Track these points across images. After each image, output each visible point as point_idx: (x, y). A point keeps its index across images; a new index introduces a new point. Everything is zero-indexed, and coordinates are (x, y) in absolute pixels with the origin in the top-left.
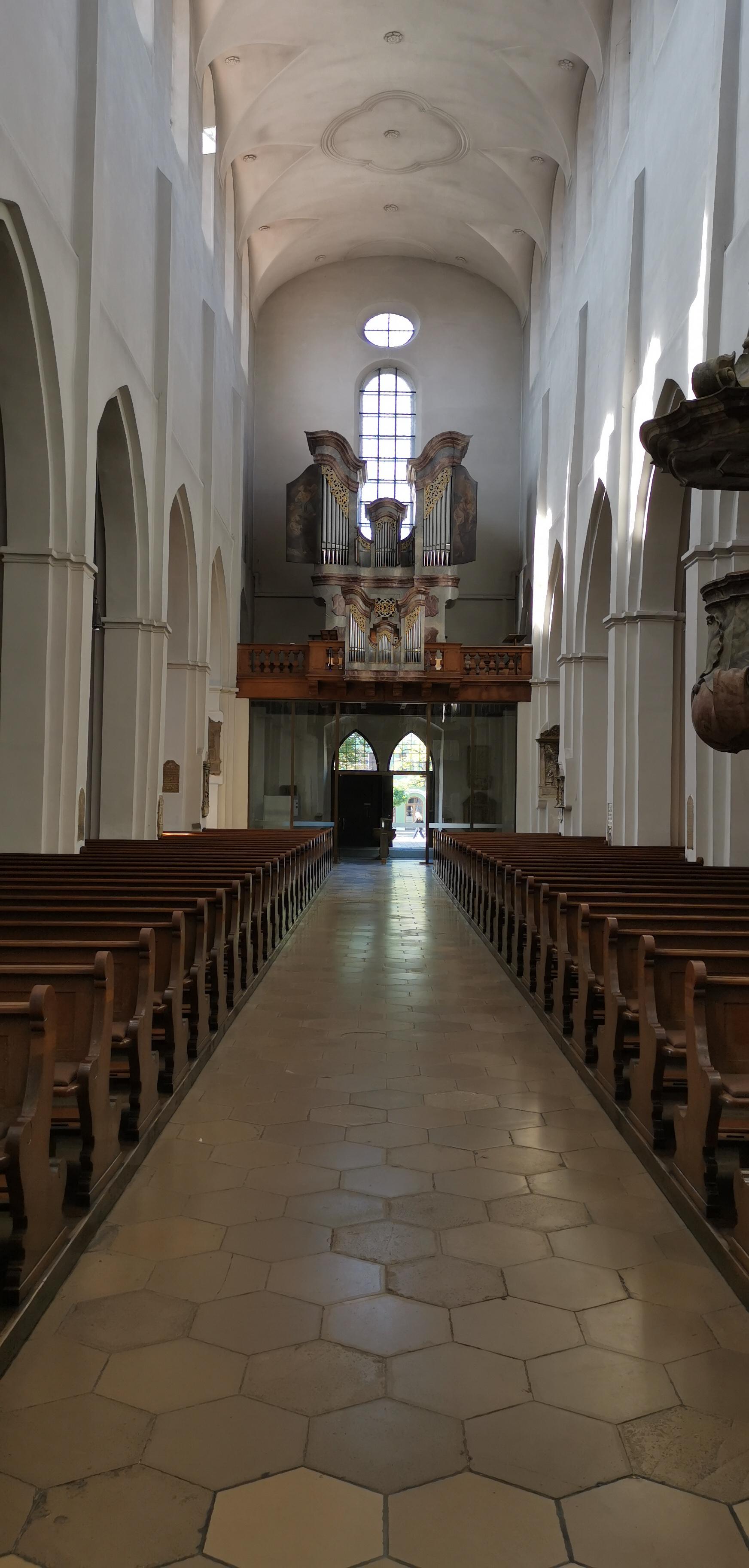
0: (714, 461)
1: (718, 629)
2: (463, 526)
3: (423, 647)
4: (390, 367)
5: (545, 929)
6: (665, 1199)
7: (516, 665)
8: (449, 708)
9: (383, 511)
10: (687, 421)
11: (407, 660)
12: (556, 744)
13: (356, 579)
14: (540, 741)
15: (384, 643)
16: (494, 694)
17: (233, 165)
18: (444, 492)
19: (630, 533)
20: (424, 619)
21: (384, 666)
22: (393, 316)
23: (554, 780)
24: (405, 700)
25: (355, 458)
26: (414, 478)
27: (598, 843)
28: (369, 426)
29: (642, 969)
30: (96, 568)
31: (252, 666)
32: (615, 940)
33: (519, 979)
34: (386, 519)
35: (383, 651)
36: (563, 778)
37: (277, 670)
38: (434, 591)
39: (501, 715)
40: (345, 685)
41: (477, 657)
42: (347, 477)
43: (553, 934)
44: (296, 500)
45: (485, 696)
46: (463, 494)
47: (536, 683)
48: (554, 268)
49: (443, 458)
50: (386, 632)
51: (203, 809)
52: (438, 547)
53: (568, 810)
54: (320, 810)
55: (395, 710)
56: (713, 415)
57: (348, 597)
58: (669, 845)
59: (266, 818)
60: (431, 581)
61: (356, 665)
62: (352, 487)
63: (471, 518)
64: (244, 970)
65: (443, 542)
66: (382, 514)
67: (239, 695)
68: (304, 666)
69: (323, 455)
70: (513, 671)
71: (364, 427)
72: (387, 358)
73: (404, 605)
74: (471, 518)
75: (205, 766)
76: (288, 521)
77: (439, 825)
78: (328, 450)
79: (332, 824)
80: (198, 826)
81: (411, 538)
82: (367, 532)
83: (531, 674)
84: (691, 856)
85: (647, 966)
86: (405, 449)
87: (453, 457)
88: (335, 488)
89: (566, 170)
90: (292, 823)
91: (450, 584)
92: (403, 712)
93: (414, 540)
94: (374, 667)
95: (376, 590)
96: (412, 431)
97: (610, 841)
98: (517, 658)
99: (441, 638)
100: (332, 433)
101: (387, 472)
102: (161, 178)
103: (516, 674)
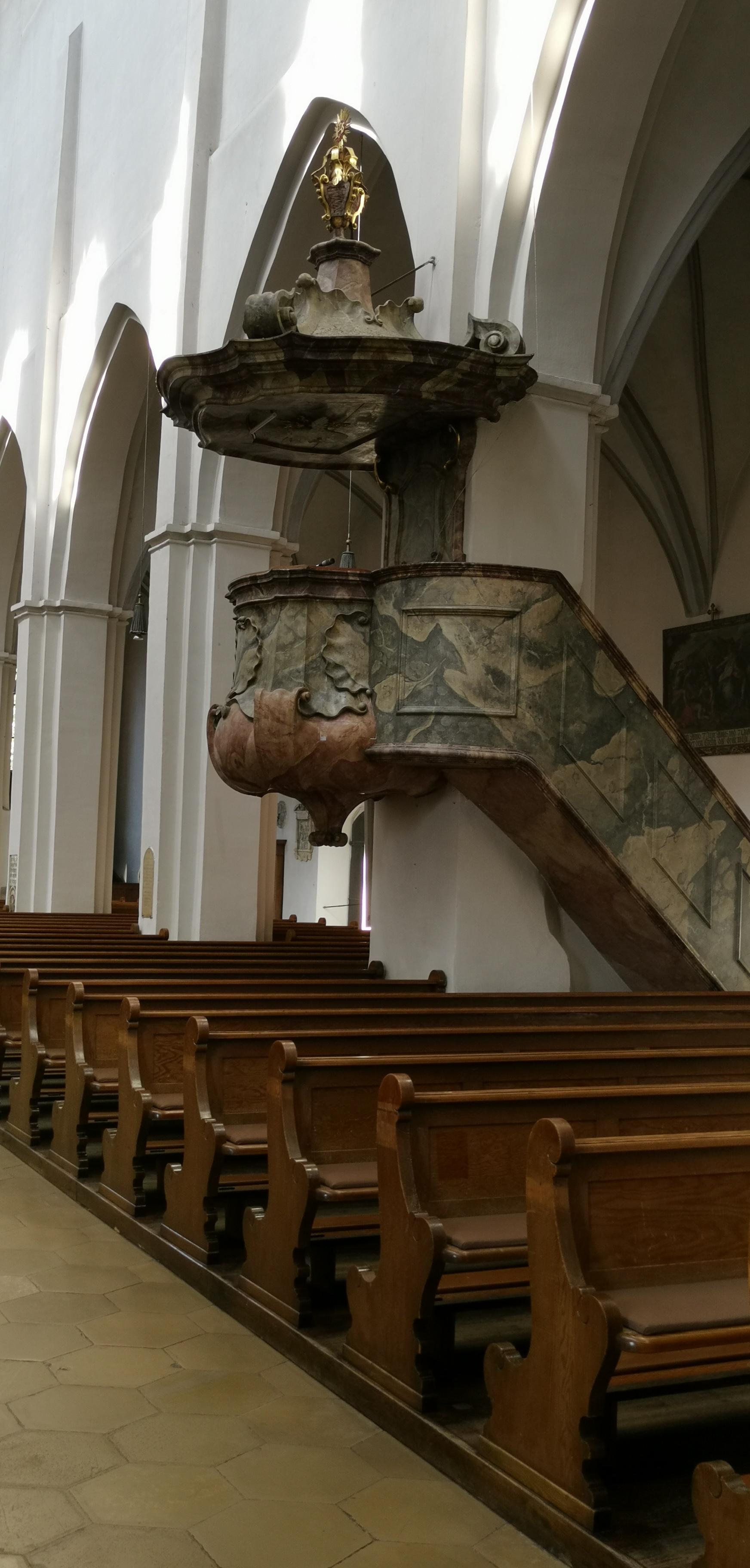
0: (250, 422)
1: (255, 636)
6: (333, 1396)
10: (235, 365)
19: (54, 498)
58: (91, 911)
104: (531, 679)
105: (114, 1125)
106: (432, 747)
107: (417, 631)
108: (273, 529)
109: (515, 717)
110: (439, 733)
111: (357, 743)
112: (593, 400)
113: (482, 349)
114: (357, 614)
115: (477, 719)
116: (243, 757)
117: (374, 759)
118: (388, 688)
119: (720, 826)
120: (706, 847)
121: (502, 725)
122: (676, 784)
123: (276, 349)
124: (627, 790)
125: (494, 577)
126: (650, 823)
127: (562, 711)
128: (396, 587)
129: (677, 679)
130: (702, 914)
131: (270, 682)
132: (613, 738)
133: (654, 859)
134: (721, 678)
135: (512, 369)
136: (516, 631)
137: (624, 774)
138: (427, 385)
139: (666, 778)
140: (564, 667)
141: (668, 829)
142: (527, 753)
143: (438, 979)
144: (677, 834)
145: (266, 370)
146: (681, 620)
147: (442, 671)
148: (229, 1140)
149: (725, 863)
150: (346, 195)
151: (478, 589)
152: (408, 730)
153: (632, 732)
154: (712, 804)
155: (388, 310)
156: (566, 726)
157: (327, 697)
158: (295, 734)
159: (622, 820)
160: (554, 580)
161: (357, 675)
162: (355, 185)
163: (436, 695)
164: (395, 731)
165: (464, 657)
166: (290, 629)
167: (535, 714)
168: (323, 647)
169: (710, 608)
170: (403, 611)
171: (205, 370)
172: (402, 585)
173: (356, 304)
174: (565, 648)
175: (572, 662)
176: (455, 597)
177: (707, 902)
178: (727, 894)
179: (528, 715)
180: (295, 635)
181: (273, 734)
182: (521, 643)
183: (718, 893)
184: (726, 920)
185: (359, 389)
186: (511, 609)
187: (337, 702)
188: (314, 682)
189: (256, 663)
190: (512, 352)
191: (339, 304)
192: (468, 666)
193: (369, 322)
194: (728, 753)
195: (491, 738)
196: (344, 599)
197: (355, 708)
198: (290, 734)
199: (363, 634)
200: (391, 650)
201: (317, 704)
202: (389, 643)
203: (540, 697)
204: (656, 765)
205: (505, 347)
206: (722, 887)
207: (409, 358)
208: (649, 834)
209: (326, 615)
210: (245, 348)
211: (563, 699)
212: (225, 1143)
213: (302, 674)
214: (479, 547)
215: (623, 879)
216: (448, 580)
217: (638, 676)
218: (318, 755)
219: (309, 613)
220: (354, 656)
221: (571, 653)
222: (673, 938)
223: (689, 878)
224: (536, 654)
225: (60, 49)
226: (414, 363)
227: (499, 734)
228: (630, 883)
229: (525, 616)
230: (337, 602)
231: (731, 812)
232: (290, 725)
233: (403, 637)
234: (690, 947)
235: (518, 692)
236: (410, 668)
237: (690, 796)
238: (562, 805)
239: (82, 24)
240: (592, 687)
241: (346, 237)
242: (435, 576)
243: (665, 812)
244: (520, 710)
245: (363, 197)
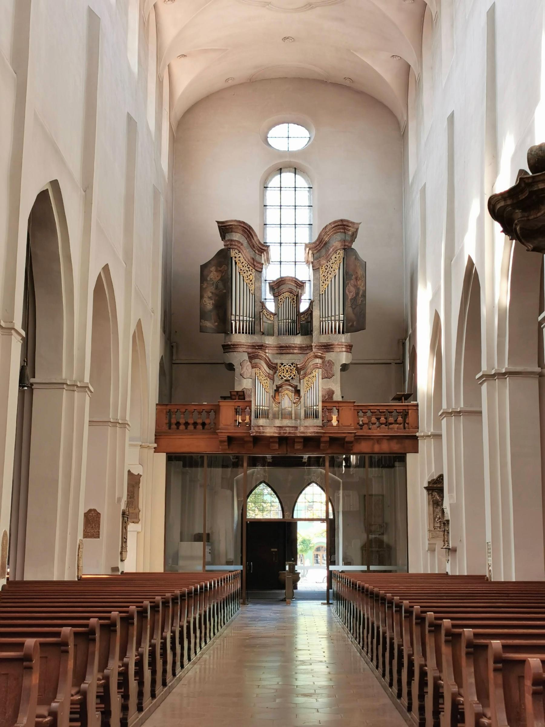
2: (354, 299)
3: (320, 404)
4: (290, 167)
5: (417, 648)
7: (405, 422)
8: (347, 460)
9: (284, 288)
10: (526, 194)
11: (306, 416)
12: (441, 491)
13: (262, 347)
14: (427, 489)
15: (287, 401)
16: (385, 447)
17: (155, 6)
18: (337, 271)
20: (320, 380)
21: (286, 422)
22: (291, 125)
23: (441, 524)
24: (305, 452)
25: (260, 243)
26: (311, 259)
27: (482, 579)
28: (272, 216)
29: (491, 674)
30: (23, 333)
31: (170, 424)
32: (500, 665)
33: (398, 701)
34: (287, 294)
35: (285, 409)
36: (448, 521)
37: (191, 427)
38: (329, 356)
39: (393, 466)
40: (251, 439)
41: (369, 414)
42: (253, 259)
43: (424, 654)
44: (209, 279)
45: (377, 448)
46: (353, 272)
47: (423, 437)
48: (426, 85)
49: (336, 242)
50: (287, 392)
51: (121, 553)
52: (333, 318)
53: (452, 551)
54: (231, 556)
55: (298, 463)
57: (253, 361)
59: (181, 563)
60: (327, 347)
61: (262, 422)
62: (257, 267)
63: (361, 293)
64: (140, 694)
65: (337, 313)
66: (284, 290)
67: (156, 450)
68: (215, 423)
69: (232, 240)
70: (402, 426)
71: (267, 218)
72: (287, 160)
73: (302, 368)
74: (361, 293)
75: (124, 513)
76: (202, 297)
77: (339, 567)
78: (237, 236)
79: (240, 568)
80: (116, 569)
81: (309, 312)
82: (271, 306)
83: (418, 428)
85: (495, 670)
86: (305, 236)
87: (345, 241)
88: (242, 269)
90: (204, 567)
91: (344, 349)
92: (303, 464)
93: (312, 312)
94: (278, 423)
95: (279, 356)
96: (310, 220)
97: (490, 577)
98: (405, 415)
99: (337, 397)
100: (239, 222)
101: (288, 256)
102: (91, 14)
103: (405, 428)
105: (443, 712)
148: (486, 716)
210: (530, 181)
212: (482, 718)
225: (482, 21)
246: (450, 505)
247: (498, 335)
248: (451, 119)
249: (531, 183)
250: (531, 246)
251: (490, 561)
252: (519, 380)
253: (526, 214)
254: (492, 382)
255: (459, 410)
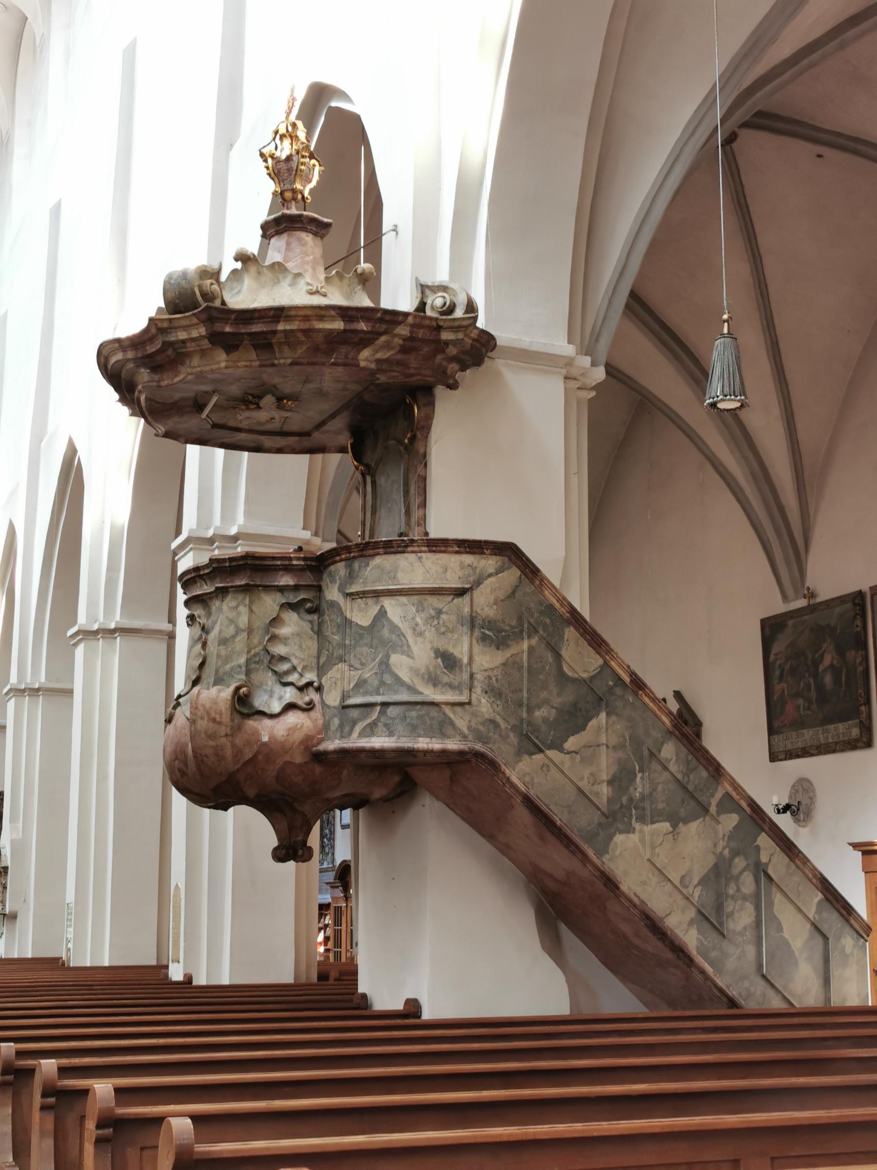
27: (55, 963)
29: (36, 1115)
32: (52, 1100)
36: (6, 869)
48: (19, 150)
56: (193, 340)
84: (176, 973)
89: (35, 25)
104: (487, 660)
106: (379, 742)
107: (361, 615)
108: (304, 529)
109: (469, 703)
110: (386, 725)
111: (302, 742)
112: (569, 362)
113: (429, 312)
114: (304, 601)
115: (426, 708)
116: (186, 765)
117: (320, 757)
118: (334, 680)
119: (731, 821)
120: (715, 845)
121: (454, 713)
122: (672, 773)
123: (197, 324)
124: (610, 783)
125: (441, 552)
126: (642, 819)
127: (525, 695)
128: (340, 569)
129: (777, 672)
130: (712, 919)
131: (212, 680)
132: (590, 724)
133: (649, 860)
134: (821, 668)
135: (457, 332)
136: (467, 610)
137: (605, 765)
138: (365, 353)
139: (659, 768)
140: (525, 646)
141: (666, 826)
142: (484, 743)
143: (413, 1008)
144: (677, 830)
145: (191, 347)
146: (779, 607)
147: (388, 657)
149: (740, 863)
150: (295, 168)
151: (424, 566)
152: (354, 723)
153: (614, 718)
154: (719, 795)
155: (336, 280)
156: (530, 711)
157: (271, 694)
158: (232, 735)
159: (607, 817)
160: (508, 552)
161: (305, 668)
162: (303, 157)
163: (382, 683)
164: (341, 726)
165: (411, 640)
166: (231, 621)
167: (492, 699)
168: (267, 638)
169: (806, 592)
170: (347, 594)
171: (134, 352)
172: (346, 567)
173: (298, 275)
174: (526, 625)
175: (534, 641)
176: (400, 575)
177: (719, 908)
178: (745, 898)
179: (483, 701)
180: (237, 627)
181: (212, 736)
182: (472, 622)
183: (733, 897)
184: (745, 928)
185: (289, 361)
186: (460, 586)
187: (281, 698)
188: (256, 678)
189: (200, 661)
190: (459, 313)
191: (281, 276)
192: (415, 649)
193: (311, 293)
194: (834, 751)
195: (443, 728)
196: (288, 586)
197: (300, 703)
198: (226, 735)
199: (311, 622)
200: (336, 637)
201: (260, 702)
202: (334, 630)
203: (497, 680)
204: (646, 753)
205: (451, 309)
206: (738, 890)
207: (339, 325)
208: (641, 831)
209: (270, 603)
210: (165, 325)
211: (525, 682)
213: (244, 669)
214: (442, 521)
215: (610, 883)
216: (391, 558)
217: (616, 654)
218: (260, 757)
219: (251, 603)
220: (300, 647)
221: (533, 631)
222: (679, 950)
223: (695, 881)
224: (491, 634)
226: (345, 331)
227: (451, 723)
228: (618, 888)
229: (477, 593)
230: (281, 589)
231: (744, 804)
232: (226, 726)
233: (347, 623)
234: (700, 960)
235: (472, 676)
236: (355, 656)
237: (690, 787)
238: (529, 802)
239: (135, 40)
240: (562, 667)
241: (297, 209)
242: (378, 554)
243: (660, 806)
244: (474, 696)
245: (317, 169)
246: (12, 841)
247: (108, 569)
248: (56, 212)
249: (168, 328)
250: (162, 429)
251: (70, 933)
252: (136, 642)
253: (156, 377)
254: (93, 643)
255: (37, 686)
